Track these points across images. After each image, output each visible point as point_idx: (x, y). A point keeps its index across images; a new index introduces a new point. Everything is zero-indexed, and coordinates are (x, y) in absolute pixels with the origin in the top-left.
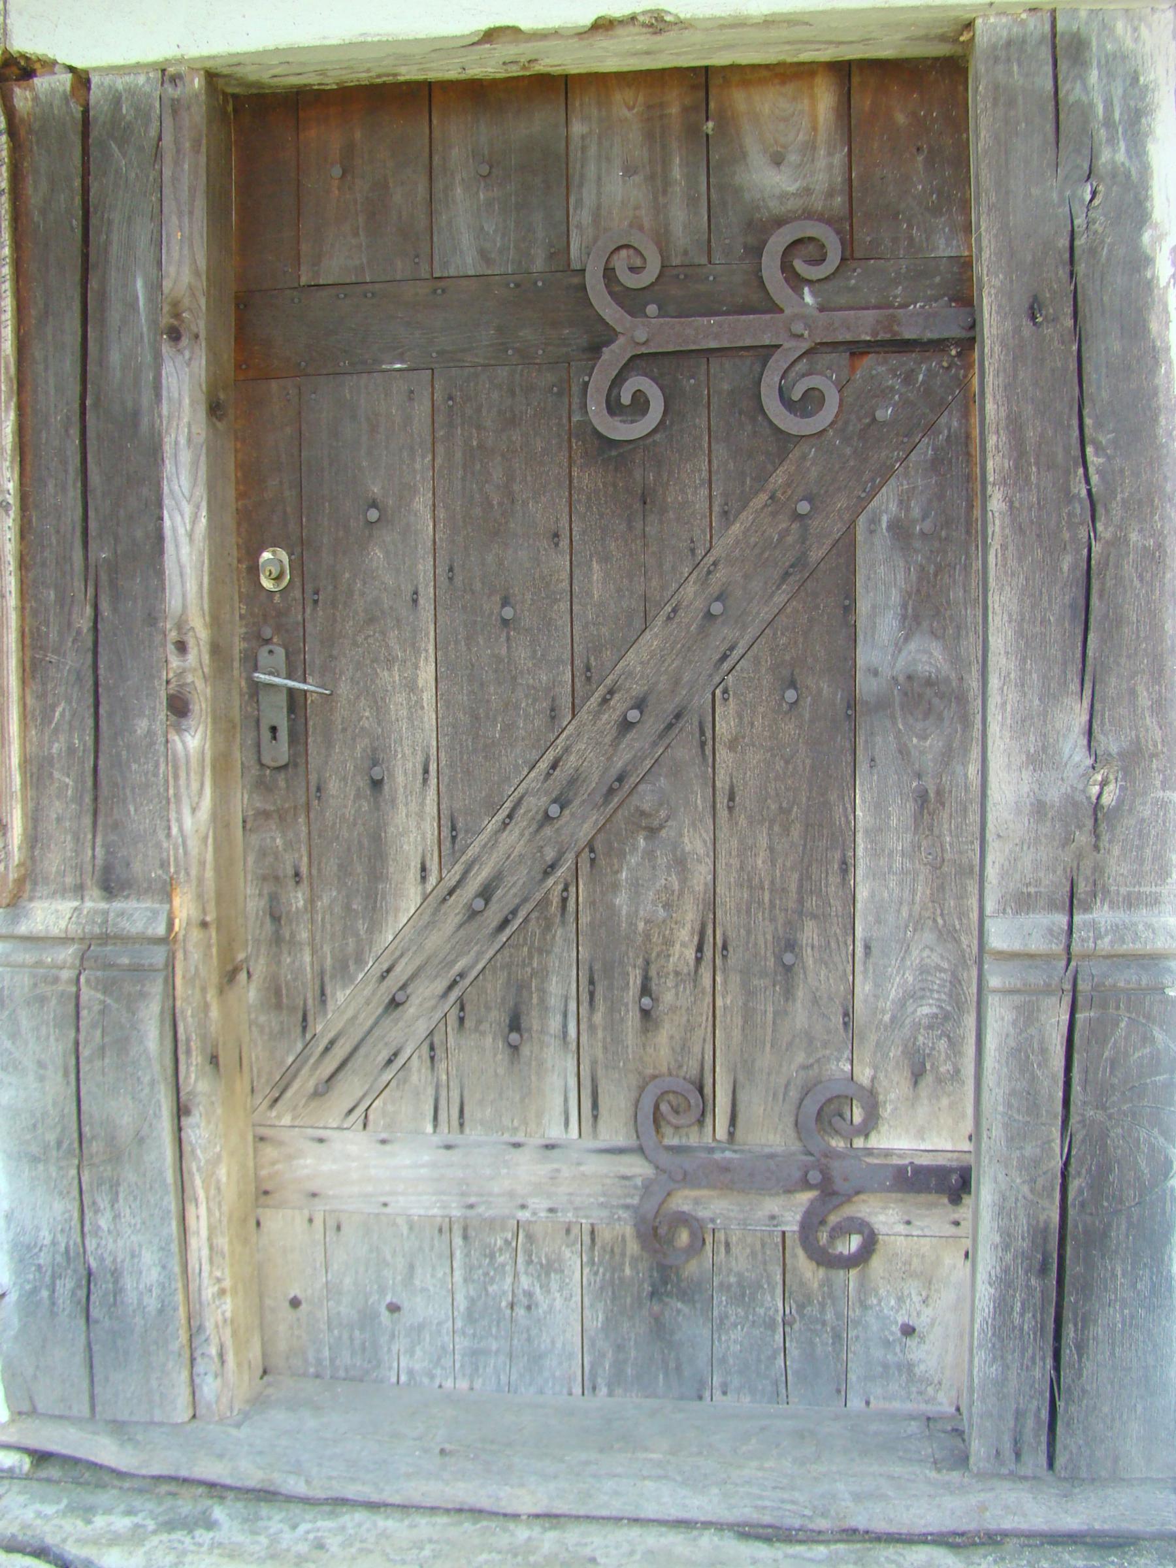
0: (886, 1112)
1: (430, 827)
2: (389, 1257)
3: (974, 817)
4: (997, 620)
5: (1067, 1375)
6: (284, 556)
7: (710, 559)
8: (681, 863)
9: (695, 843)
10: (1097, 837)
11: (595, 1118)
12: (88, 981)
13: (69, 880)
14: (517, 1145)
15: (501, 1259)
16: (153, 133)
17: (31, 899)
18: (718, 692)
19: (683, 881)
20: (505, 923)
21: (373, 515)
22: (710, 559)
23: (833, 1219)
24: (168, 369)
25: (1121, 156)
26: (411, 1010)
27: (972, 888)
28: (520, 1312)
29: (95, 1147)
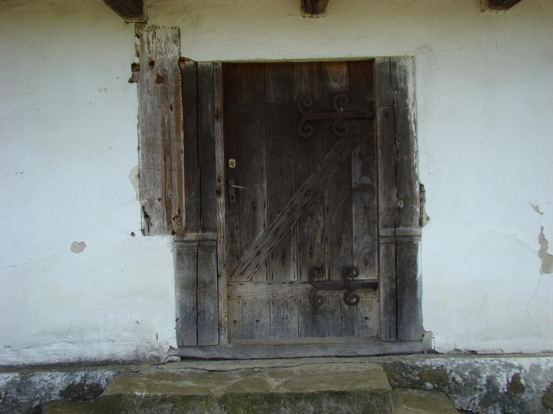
0: (360, 272)
1: (266, 217)
2: (256, 309)
3: (376, 212)
4: (380, 174)
5: (399, 320)
6: (234, 160)
7: (323, 161)
8: (318, 223)
9: (320, 218)
10: (400, 214)
11: (301, 275)
12: (200, 249)
13: (195, 229)
14: (284, 283)
15: (281, 308)
16: (212, 75)
17: (186, 233)
18: (325, 188)
19: (318, 226)
20: (282, 236)
21: (253, 152)
22: (323, 161)
23: (350, 295)
24: (216, 124)
25: (403, 85)
26: (261, 255)
27: (376, 225)
28: (285, 319)
29: (200, 285)
